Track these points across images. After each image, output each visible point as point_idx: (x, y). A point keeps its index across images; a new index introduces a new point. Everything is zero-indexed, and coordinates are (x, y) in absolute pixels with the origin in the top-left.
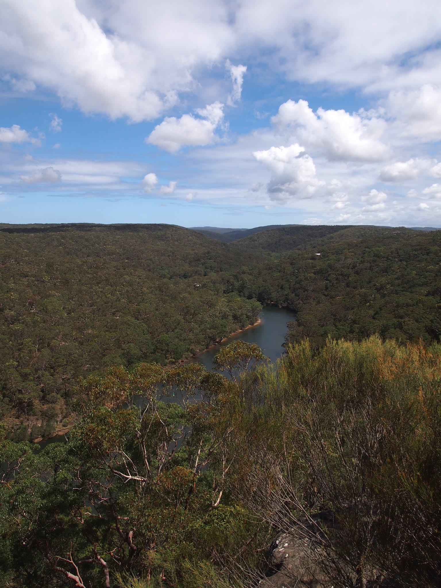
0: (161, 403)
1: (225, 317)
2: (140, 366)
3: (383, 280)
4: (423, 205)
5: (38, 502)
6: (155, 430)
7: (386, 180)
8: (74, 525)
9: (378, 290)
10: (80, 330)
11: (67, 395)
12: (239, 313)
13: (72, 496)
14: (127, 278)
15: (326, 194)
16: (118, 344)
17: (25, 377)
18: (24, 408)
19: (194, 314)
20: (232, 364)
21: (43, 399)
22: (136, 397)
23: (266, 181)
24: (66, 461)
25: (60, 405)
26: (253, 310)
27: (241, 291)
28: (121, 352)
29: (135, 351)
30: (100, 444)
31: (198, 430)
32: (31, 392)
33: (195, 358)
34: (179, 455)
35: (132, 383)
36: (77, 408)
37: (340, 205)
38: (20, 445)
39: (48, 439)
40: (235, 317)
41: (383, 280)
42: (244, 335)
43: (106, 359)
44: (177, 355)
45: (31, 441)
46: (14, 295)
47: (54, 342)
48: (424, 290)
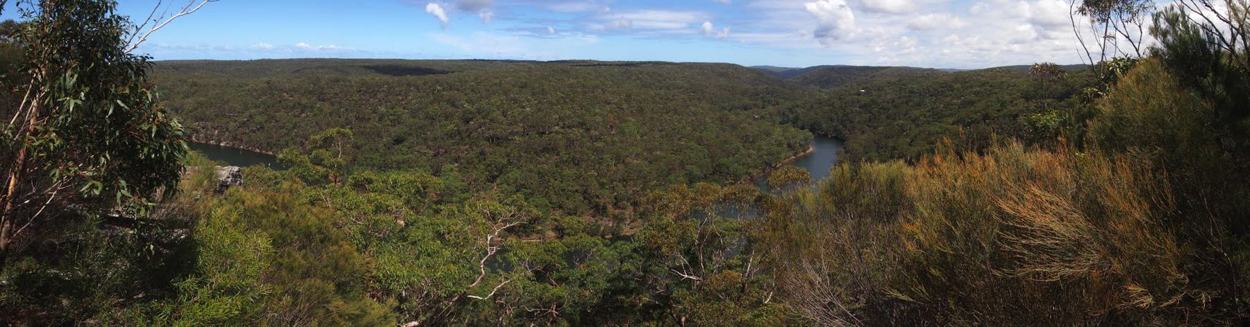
0: (719, 218)
1: (780, 144)
2: (700, 185)
3: (916, 113)
4: (946, 51)
5: (604, 285)
6: (711, 241)
7: (914, 29)
8: (633, 305)
9: (913, 121)
10: (650, 151)
11: (635, 204)
12: (792, 142)
13: (633, 285)
14: (693, 109)
15: (867, 40)
16: (682, 165)
17: (602, 185)
18: (599, 210)
19: (753, 142)
20: (782, 186)
21: (616, 205)
22: (696, 211)
23: (814, 27)
24: (630, 257)
25: (629, 212)
26: (806, 140)
27: (795, 122)
28: (684, 172)
29: (697, 171)
30: (659, 248)
31: (751, 241)
32: (606, 198)
33: (752, 180)
34: (733, 261)
35: (693, 199)
36: (642, 215)
37: (877, 49)
38: (594, 239)
39: (616, 237)
40: (789, 145)
41: (916, 113)
42: (797, 161)
43: (672, 177)
44: (736, 178)
45: (603, 237)
46: (599, 119)
47: (628, 160)
48: (951, 120)
